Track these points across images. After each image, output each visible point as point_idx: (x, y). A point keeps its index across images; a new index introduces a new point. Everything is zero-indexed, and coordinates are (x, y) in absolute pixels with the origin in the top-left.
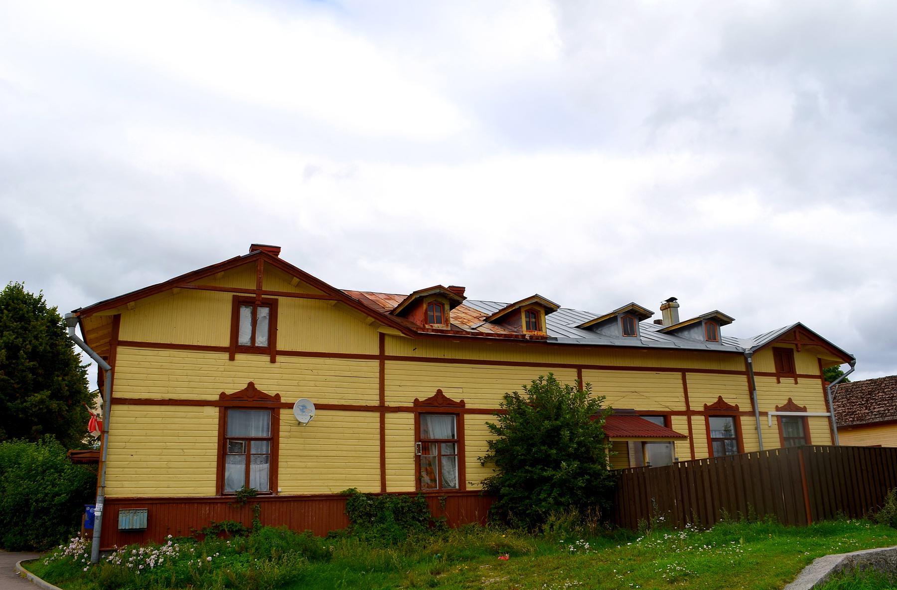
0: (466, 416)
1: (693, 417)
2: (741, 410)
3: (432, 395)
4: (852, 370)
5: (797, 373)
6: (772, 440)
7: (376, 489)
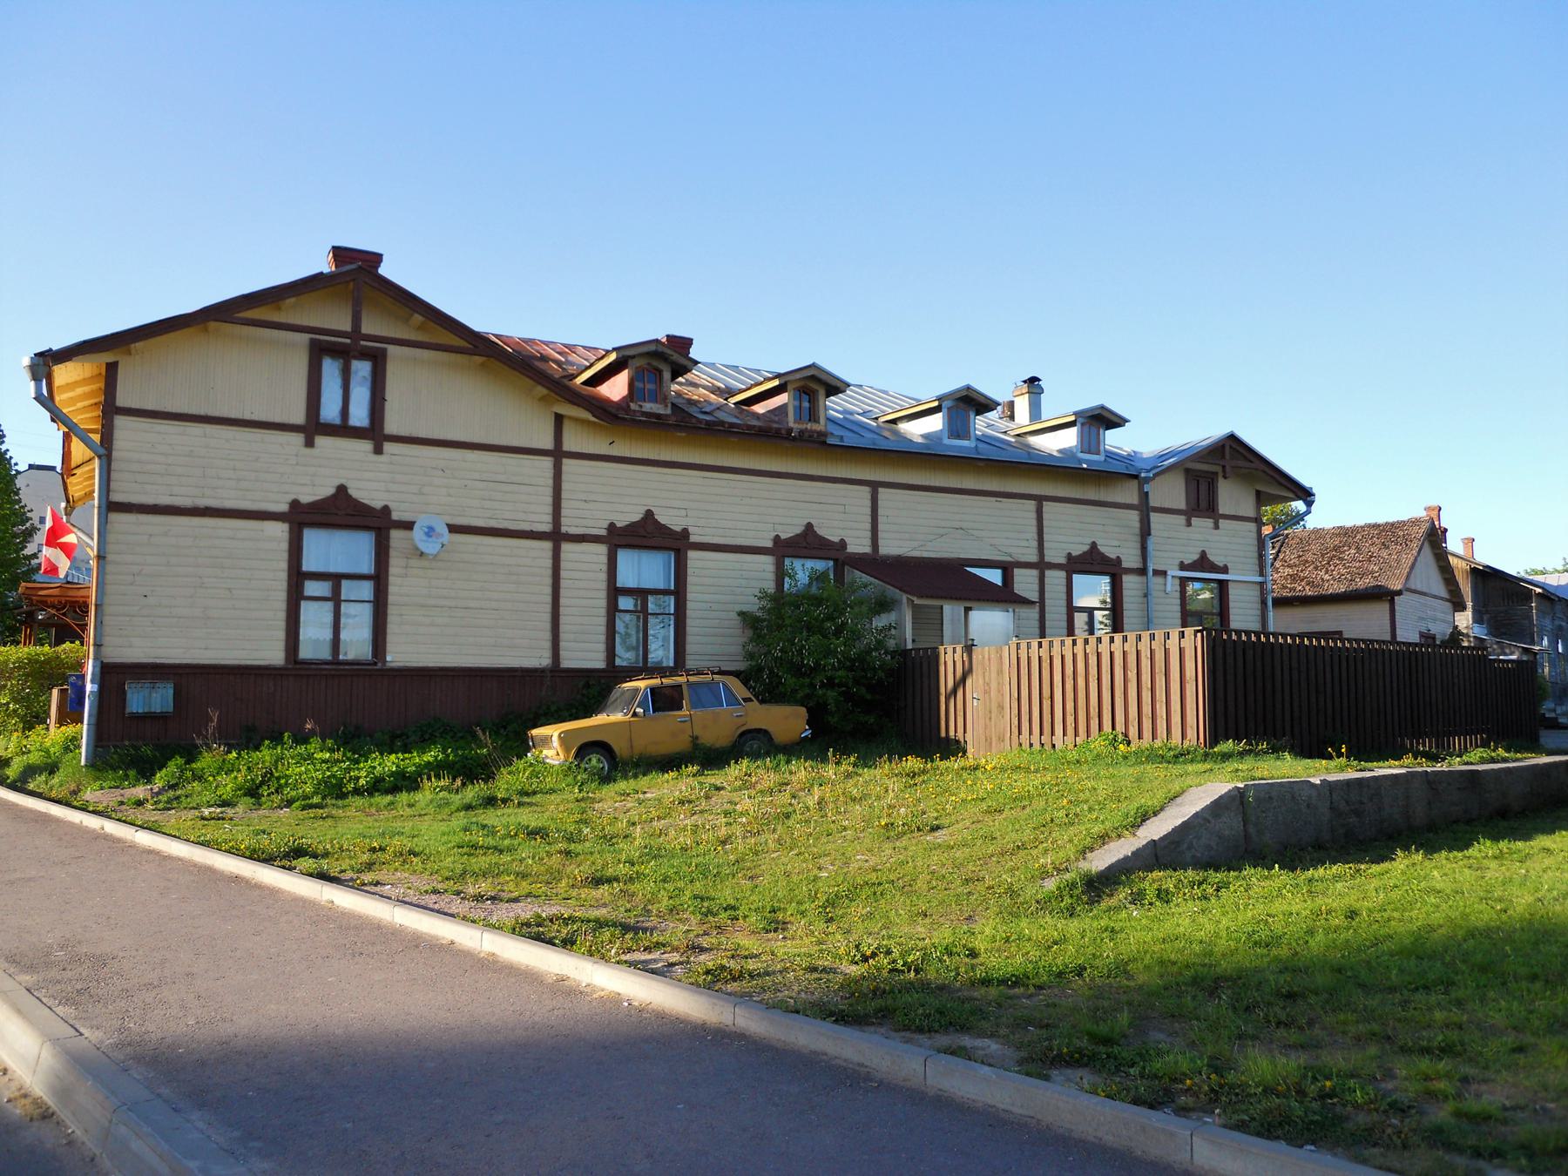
0: (692, 554)
2: (1125, 565)
5: (1221, 512)
7: (539, 658)
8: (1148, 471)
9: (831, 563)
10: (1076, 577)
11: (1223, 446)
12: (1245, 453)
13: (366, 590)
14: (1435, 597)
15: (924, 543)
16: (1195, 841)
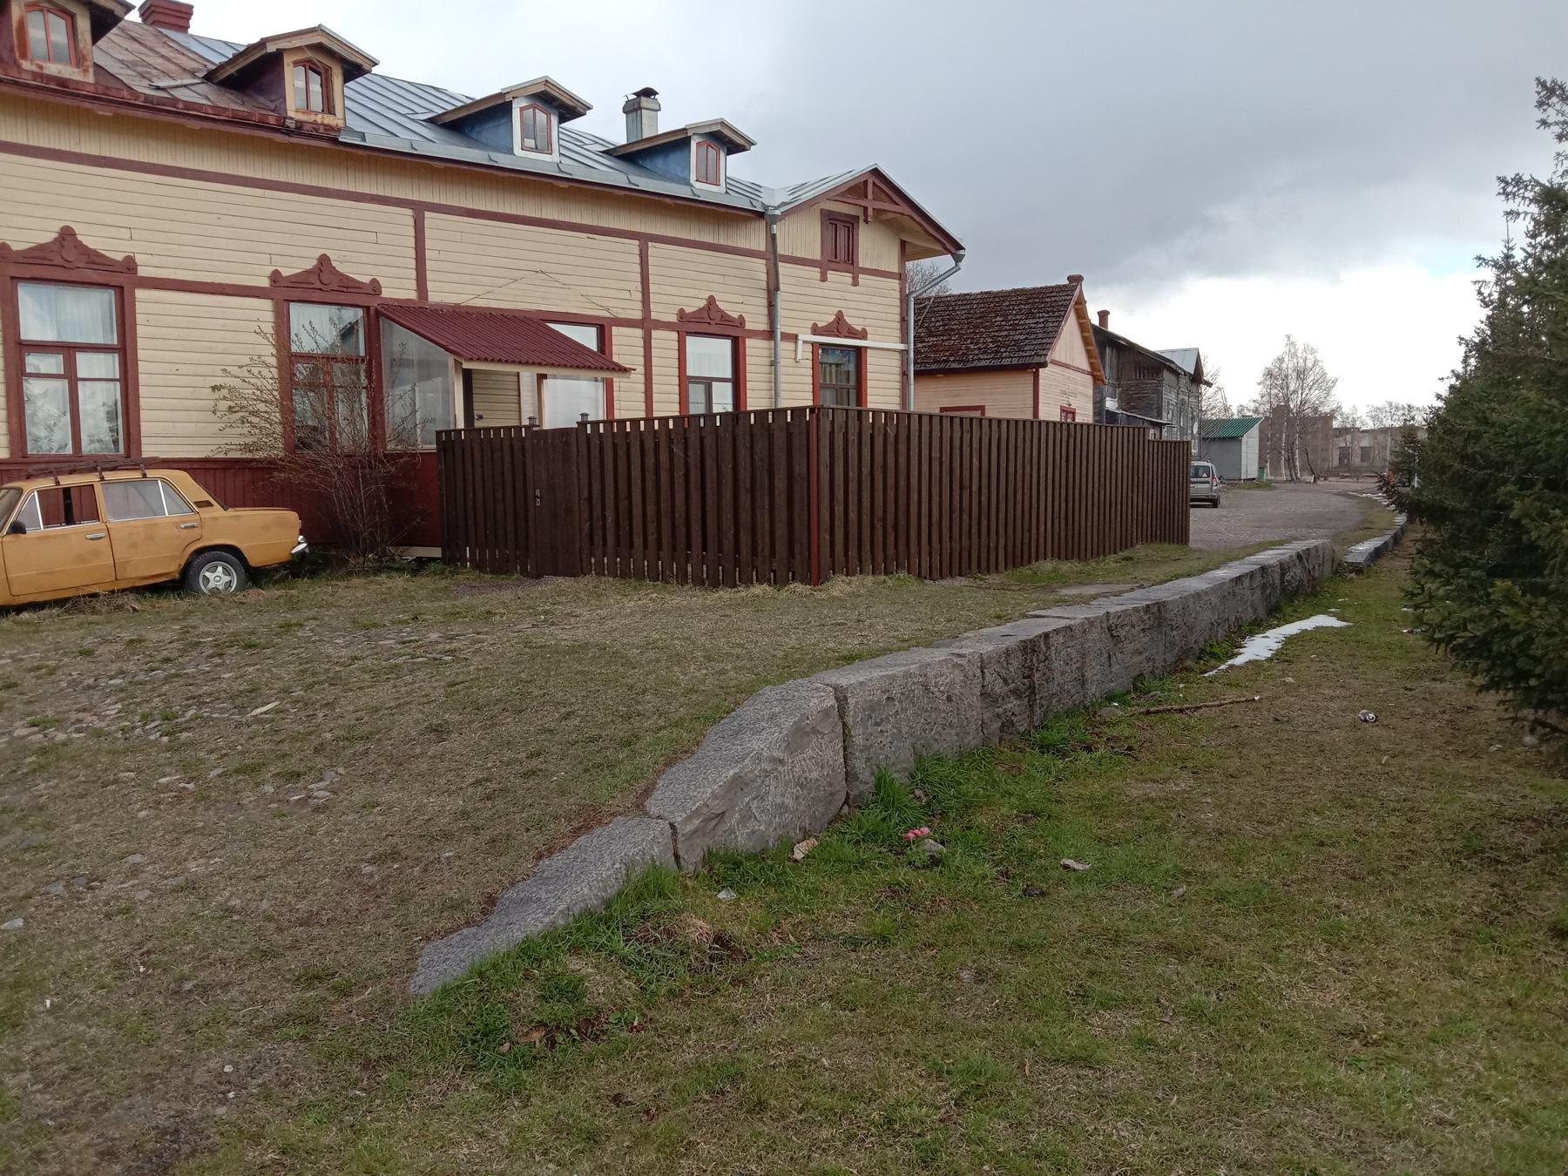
0: (140, 294)
1: (655, 334)
2: (748, 326)
3: (48, 237)
4: (956, 269)
5: (861, 265)
6: (797, 392)
8: (776, 208)
9: (360, 312)
10: (690, 340)
11: (866, 183)
12: (889, 192)
13: (107, 365)
14: (1077, 370)
15: (491, 289)
16: (754, 805)
